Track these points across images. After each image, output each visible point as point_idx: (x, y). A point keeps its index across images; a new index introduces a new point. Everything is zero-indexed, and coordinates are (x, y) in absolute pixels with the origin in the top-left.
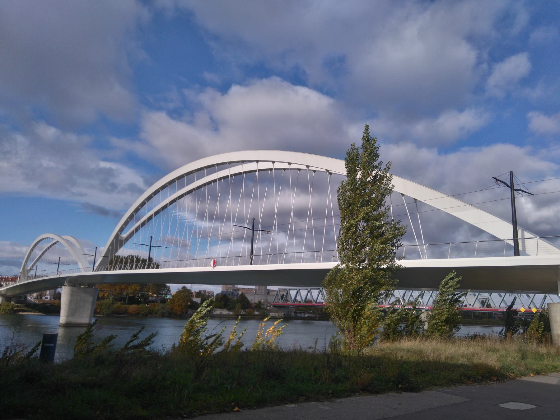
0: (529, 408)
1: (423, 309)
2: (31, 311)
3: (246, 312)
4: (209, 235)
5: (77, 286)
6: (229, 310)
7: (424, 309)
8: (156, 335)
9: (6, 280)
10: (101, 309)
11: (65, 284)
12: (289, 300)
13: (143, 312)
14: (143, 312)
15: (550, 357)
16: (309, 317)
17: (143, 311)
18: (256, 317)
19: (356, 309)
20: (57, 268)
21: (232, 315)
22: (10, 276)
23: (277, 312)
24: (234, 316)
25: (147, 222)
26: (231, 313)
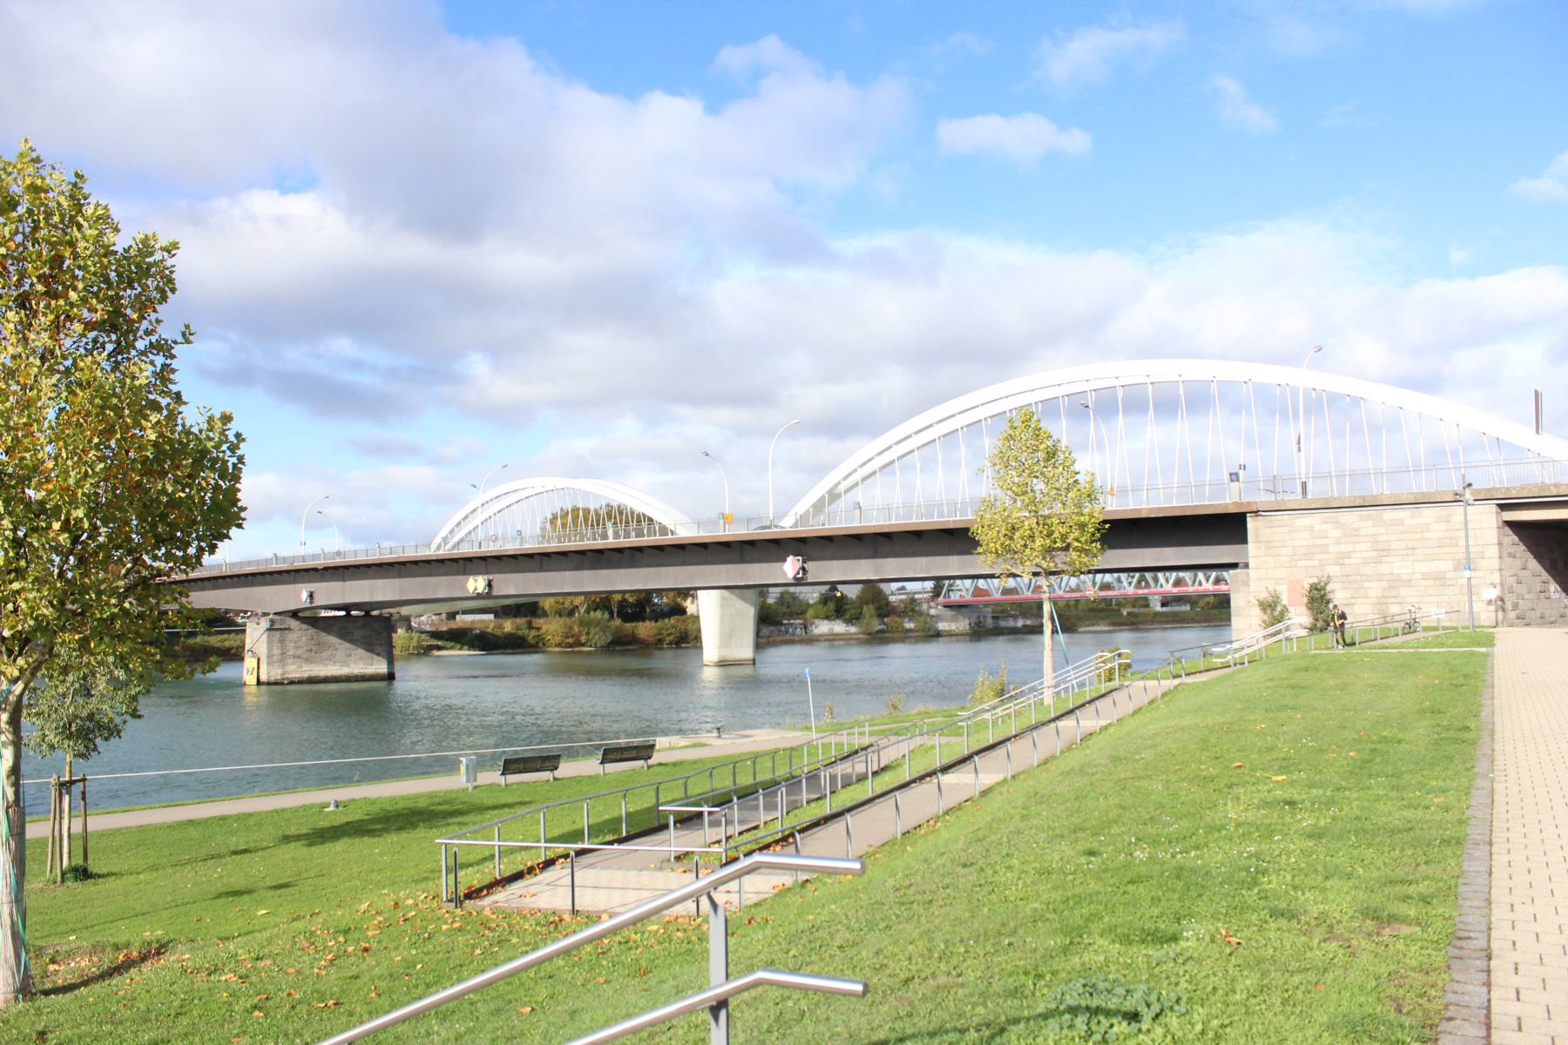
0: (493, 682)
2: (452, 648)
3: (884, 624)
6: (849, 622)
8: (894, 767)
10: (588, 634)
13: (672, 638)
14: (672, 638)
15: (1467, 729)
17: (669, 635)
18: (910, 634)
19: (397, 983)
21: (855, 634)
23: (954, 619)
24: (862, 636)
26: (853, 629)
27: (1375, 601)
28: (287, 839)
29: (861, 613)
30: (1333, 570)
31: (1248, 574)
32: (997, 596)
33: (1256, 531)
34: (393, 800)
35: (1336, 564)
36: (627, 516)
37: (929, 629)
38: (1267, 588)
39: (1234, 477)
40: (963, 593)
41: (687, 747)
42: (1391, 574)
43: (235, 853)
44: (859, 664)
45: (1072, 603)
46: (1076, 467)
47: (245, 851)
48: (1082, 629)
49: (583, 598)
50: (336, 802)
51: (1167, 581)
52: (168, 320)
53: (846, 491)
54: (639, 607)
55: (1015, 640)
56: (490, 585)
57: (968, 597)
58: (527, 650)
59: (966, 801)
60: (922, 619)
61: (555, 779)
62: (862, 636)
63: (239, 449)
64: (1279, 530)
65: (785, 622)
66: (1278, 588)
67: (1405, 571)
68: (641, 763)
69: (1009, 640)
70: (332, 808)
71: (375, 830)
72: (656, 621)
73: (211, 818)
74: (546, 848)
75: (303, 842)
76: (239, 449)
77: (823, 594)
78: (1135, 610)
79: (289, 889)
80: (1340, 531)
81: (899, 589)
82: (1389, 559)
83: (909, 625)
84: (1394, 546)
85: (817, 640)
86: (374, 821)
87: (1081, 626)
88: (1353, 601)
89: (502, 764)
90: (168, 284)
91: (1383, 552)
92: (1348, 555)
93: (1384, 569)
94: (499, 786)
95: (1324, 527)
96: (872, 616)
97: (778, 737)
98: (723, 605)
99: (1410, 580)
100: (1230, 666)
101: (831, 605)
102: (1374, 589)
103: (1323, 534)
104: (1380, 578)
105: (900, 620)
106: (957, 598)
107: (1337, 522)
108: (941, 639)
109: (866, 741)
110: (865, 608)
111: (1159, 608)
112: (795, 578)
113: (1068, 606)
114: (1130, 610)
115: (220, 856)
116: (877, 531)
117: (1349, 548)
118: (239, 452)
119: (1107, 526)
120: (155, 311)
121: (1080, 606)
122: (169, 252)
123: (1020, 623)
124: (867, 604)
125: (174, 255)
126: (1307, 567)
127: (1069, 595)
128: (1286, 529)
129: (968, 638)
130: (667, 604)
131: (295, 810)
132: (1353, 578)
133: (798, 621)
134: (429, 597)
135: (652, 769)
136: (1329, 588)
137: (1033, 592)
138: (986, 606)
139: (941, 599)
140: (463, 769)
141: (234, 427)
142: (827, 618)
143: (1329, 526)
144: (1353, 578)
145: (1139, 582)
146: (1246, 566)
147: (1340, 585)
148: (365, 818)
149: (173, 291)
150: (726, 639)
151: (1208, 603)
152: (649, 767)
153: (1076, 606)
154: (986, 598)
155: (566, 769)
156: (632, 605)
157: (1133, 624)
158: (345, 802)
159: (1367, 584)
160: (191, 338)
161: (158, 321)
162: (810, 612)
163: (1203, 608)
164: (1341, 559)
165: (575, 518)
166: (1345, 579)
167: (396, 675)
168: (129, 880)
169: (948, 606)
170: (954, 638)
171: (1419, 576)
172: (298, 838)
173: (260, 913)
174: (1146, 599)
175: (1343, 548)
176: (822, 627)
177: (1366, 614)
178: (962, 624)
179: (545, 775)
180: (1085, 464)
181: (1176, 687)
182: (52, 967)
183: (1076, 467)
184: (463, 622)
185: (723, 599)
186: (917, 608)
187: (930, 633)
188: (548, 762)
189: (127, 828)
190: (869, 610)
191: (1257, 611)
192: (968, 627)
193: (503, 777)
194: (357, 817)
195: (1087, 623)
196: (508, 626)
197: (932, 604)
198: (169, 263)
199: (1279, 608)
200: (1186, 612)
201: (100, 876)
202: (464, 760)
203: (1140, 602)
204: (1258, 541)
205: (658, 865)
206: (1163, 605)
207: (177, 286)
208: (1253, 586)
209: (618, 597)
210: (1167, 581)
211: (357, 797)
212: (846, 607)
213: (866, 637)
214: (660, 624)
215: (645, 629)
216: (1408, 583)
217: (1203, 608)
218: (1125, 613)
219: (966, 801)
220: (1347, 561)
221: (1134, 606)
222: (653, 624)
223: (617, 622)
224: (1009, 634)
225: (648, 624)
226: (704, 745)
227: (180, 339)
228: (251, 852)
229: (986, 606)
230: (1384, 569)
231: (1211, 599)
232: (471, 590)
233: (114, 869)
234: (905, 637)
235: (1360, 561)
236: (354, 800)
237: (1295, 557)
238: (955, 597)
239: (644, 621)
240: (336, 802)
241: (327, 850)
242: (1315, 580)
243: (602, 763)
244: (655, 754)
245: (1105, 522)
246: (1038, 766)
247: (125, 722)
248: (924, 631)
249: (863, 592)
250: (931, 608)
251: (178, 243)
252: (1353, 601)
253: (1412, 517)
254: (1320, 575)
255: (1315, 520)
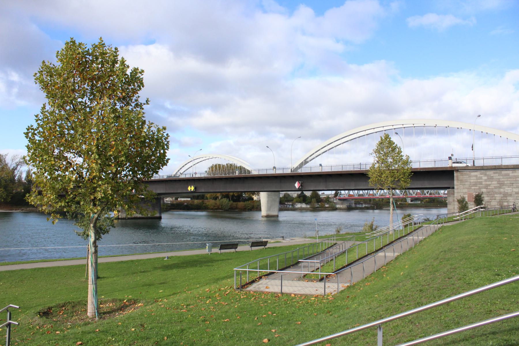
3: (319, 205)
6: (307, 204)
21: (309, 208)
23: (342, 204)
26: (308, 206)
27: (498, 201)
28: (156, 268)
29: (311, 201)
30: (484, 190)
31: (454, 191)
32: (356, 197)
33: (457, 177)
34: (185, 257)
35: (485, 188)
36: (229, 168)
37: (334, 207)
38: (460, 195)
39: (450, 158)
40: (345, 196)
41: (274, 242)
42: (505, 192)
43: (141, 272)
44: (309, 217)
45: (381, 200)
46: (402, 154)
47: (144, 272)
48: (384, 208)
49: (220, 194)
50: (167, 257)
51: (414, 193)
52: (142, 95)
53: (310, 161)
54: (237, 198)
55: (362, 211)
56: (195, 188)
57: (347, 197)
58: (202, 210)
59: (391, 261)
60: (331, 203)
61: (236, 252)
62: (311, 209)
63: (168, 139)
64: (465, 176)
65: (286, 203)
66: (464, 196)
67: (509, 191)
68: (263, 247)
69: (360, 211)
70: (166, 259)
71: (184, 266)
72: (244, 202)
73: (128, 261)
74: (259, 271)
75: (161, 270)
76: (168, 139)
77: (298, 195)
78: (402, 203)
79: (165, 284)
80: (486, 177)
81: (322, 194)
82: (504, 187)
83: (327, 206)
84: (506, 182)
85: (297, 210)
86: (183, 263)
87: (383, 207)
88: (490, 201)
89: (220, 246)
90: (141, 84)
91: (501, 184)
92: (489, 185)
93: (502, 190)
94: (219, 253)
95: (481, 176)
96: (315, 202)
97: (303, 240)
98: (268, 197)
99: (511, 194)
100: (459, 220)
101: (302, 198)
102: (498, 197)
103: (481, 178)
104: (500, 193)
105: (324, 204)
106: (343, 197)
107: (486, 174)
108: (337, 210)
109: (335, 242)
110: (313, 199)
111: (410, 202)
112: (298, 188)
113: (379, 200)
114: (400, 202)
115: (136, 273)
116: (327, 173)
117: (490, 183)
118: (167, 140)
119: (413, 174)
120: (138, 93)
121: (384, 201)
122: (141, 73)
123: (364, 206)
124: (313, 198)
125: (143, 74)
126: (475, 189)
127: (381, 197)
128: (468, 176)
129: (346, 210)
130: (247, 197)
131: (155, 259)
132: (491, 193)
133: (290, 203)
134: (175, 192)
135: (266, 249)
136: (482, 196)
137: (368, 196)
138: (352, 200)
139: (338, 197)
140: (207, 247)
141: (167, 132)
142: (300, 202)
143: (483, 175)
144: (491, 193)
145: (404, 193)
146: (453, 188)
147: (486, 195)
148: (179, 262)
149: (143, 86)
150: (269, 208)
151: (427, 201)
152: (266, 249)
153: (382, 201)
154: (353, 197)
155: (240, 248)
156: (236, 197)
157: (401, 207)
158: (170, 257)
159: (496, 195)
160: (149, 102)
161: (139, 97)
162: (295, 200)
163: (424, 203)
164: (486, 187)
165: (216, 168)
166: (488, 193)
167: (162, 218)
168: (110, 280)
169: (340, 200)
170: (341, 210)
171: (514, 193)
172: (159, 268)
173: (160, 291)
174: (406, 199)
175: (488, 183)
176: (298, 205)
177: (495, 205)
178: (344, 206)
179: (233, 250)
180: (406, 152)
181: (442, 226)
182: (101, 306)
183: (402, 154)
184: (180, 201)
185: (268, 195)
186: (330, 200)
187: (334, 208)
188: (234, 246)
189: (103, 263)
190: (314, 200)
191: (456, 203)
192: (346, 207)
193: (220, 251)
194: (176, 262)
195: (386, 206)
196: (196, 202)
197: (335, 199)
198: (141, 77)
199: (464, 202)
200: (419, 204)
201: (102, 278)
202: (208, 244)
203: (404, 200)
204: (458, 180)
205: (298, 279)
206: (411, 201)
207: (144, 85)
208: (456, 195)
209: (231, 194)
210: (414, 193)
211: (173, 256)
212: (306, 199)
213: (312, 209)
214: (245, 203)
215: (241, 204)
216: (511, 195)
217: (424, 203)
218: (399, 204)
219: (391, 261)
220: (489, 187)
221: (402, 201)
222: (243, 203)
223: (232, 202)
224: (360, 209)
225: (241, 203)
226: (280, 242)
227: (145, 103)
228: (146, 272)
229: (352, 200)
230: (502, 190)
231: (427, 200)
232: (189, 190)
233: (105, 276)
234: (323, 209)
235: (493, 187)
236: (172, 256)
237: (470, 186)
238: (342, 197)
239: (240, 202)
240: (167, 257)
241: (171, 272)
242: (477, 193)
243: (251, 247)
244: (268, 244)
245: (412, 172)
246: (409, 251)
247: (110, 229)
248: (332, 208)
249: (312, 194)
250: (334, 200)
251: (144, 70)
252: (490, 201)
253: (512, 173)
254: (479, 191)
255: (477, 173)
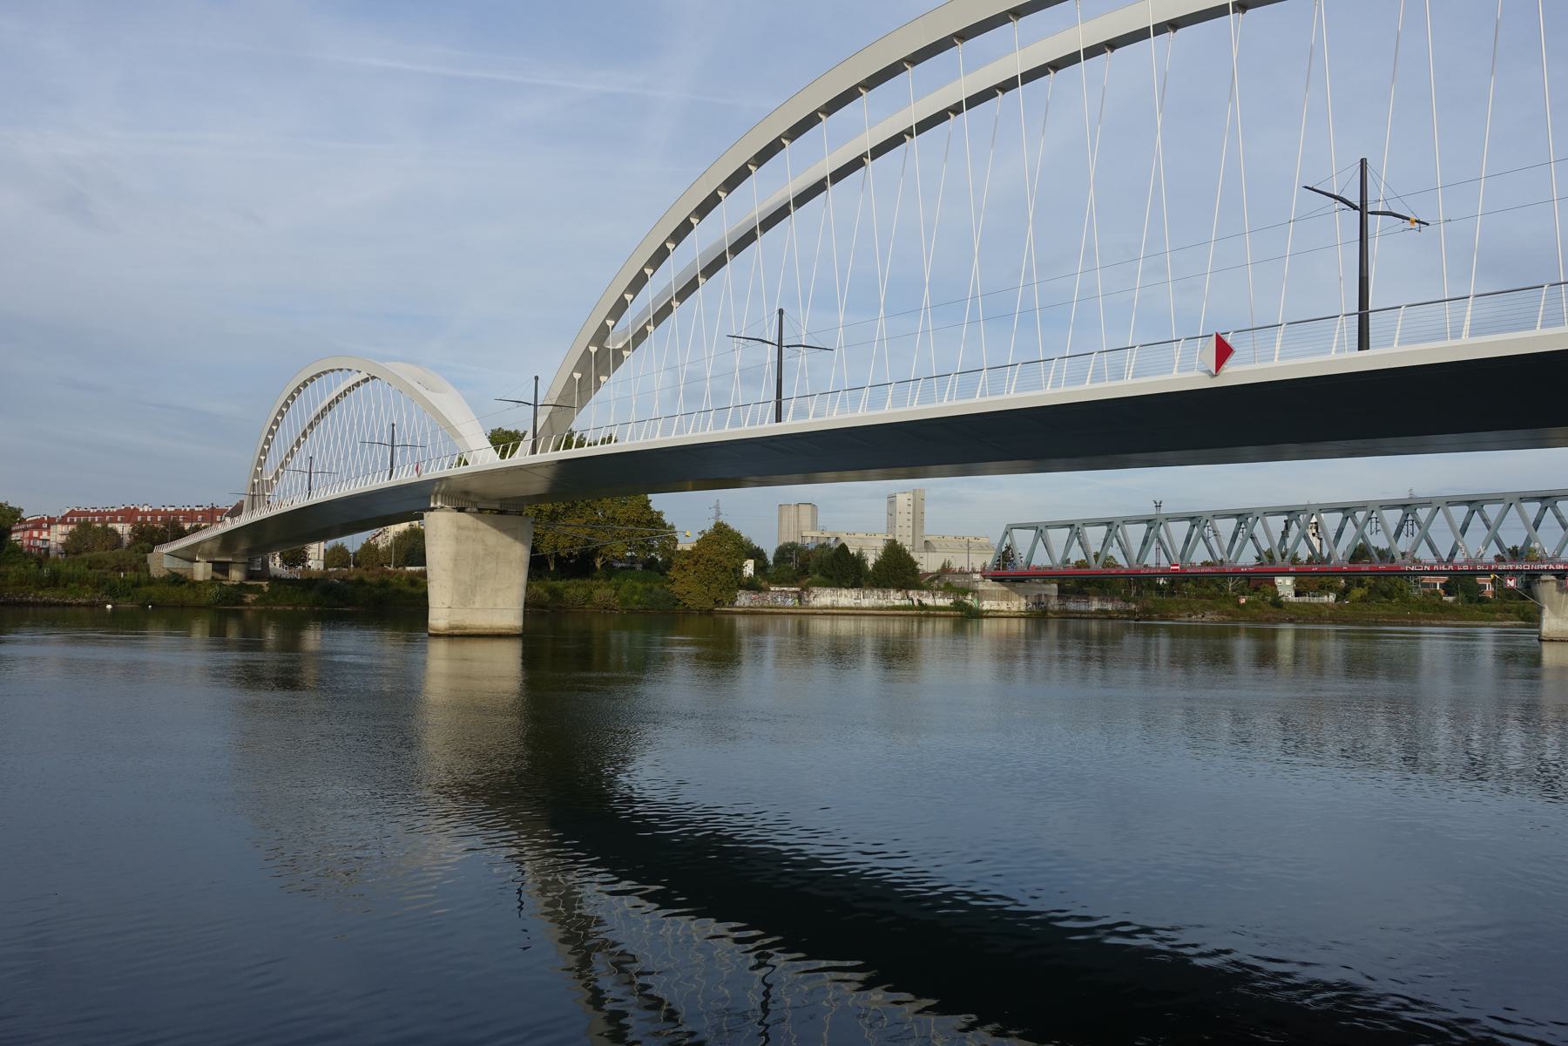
1: (1544, 570)
4: (926, 314)
5: (469, 509)
7: (1548, 570)
9: (212, 515)
11: (432, 505)
12: (1018, 560)
16: (1106, 612)
20: (795, 344)
22: (197, 506)
25: (649, 305)
